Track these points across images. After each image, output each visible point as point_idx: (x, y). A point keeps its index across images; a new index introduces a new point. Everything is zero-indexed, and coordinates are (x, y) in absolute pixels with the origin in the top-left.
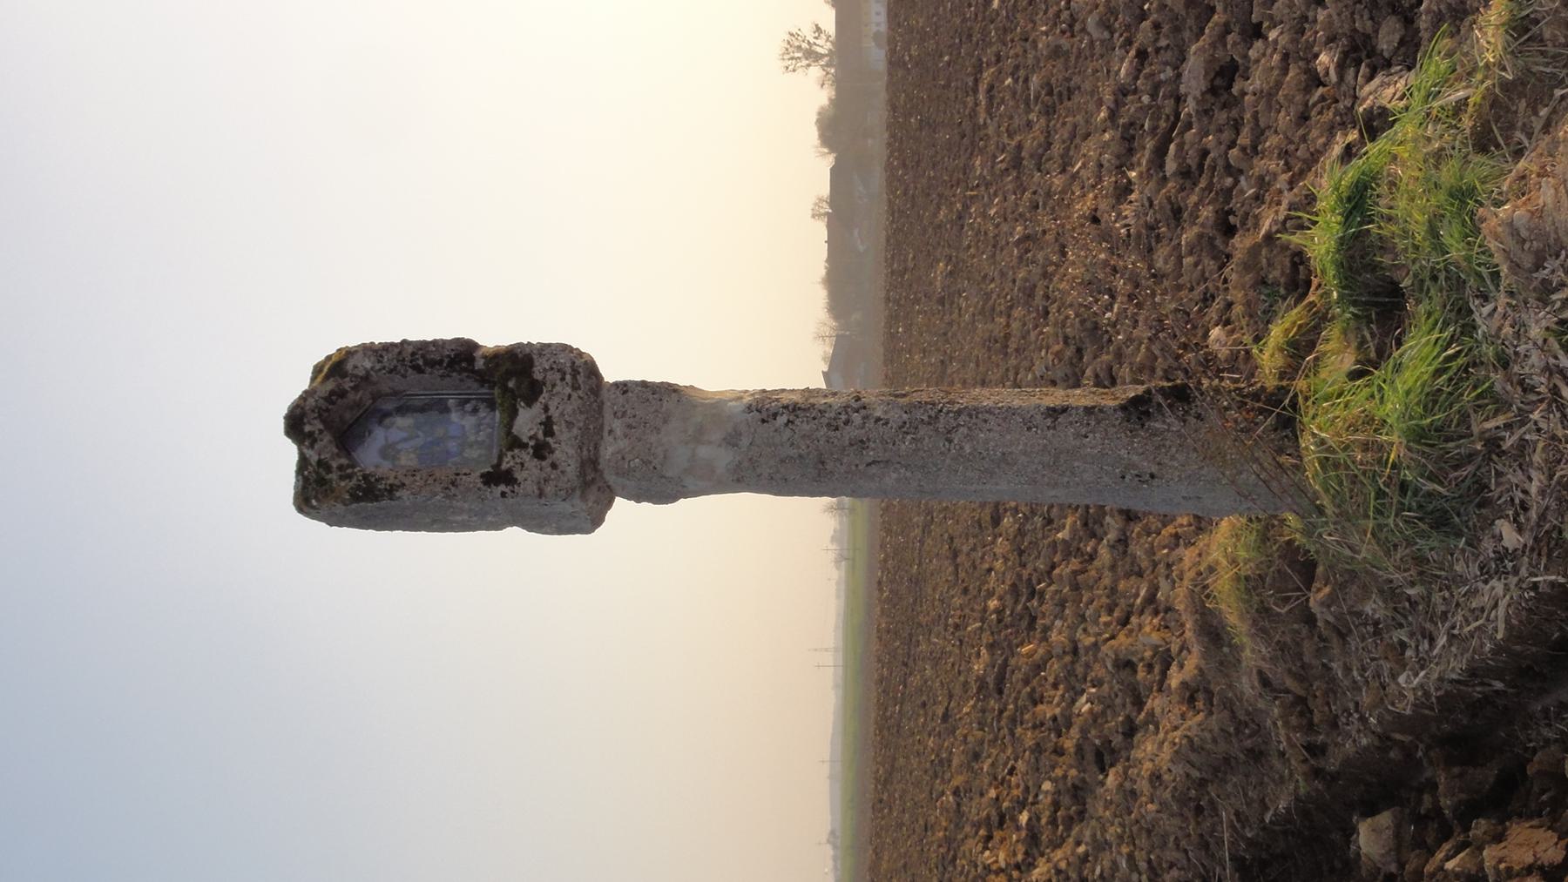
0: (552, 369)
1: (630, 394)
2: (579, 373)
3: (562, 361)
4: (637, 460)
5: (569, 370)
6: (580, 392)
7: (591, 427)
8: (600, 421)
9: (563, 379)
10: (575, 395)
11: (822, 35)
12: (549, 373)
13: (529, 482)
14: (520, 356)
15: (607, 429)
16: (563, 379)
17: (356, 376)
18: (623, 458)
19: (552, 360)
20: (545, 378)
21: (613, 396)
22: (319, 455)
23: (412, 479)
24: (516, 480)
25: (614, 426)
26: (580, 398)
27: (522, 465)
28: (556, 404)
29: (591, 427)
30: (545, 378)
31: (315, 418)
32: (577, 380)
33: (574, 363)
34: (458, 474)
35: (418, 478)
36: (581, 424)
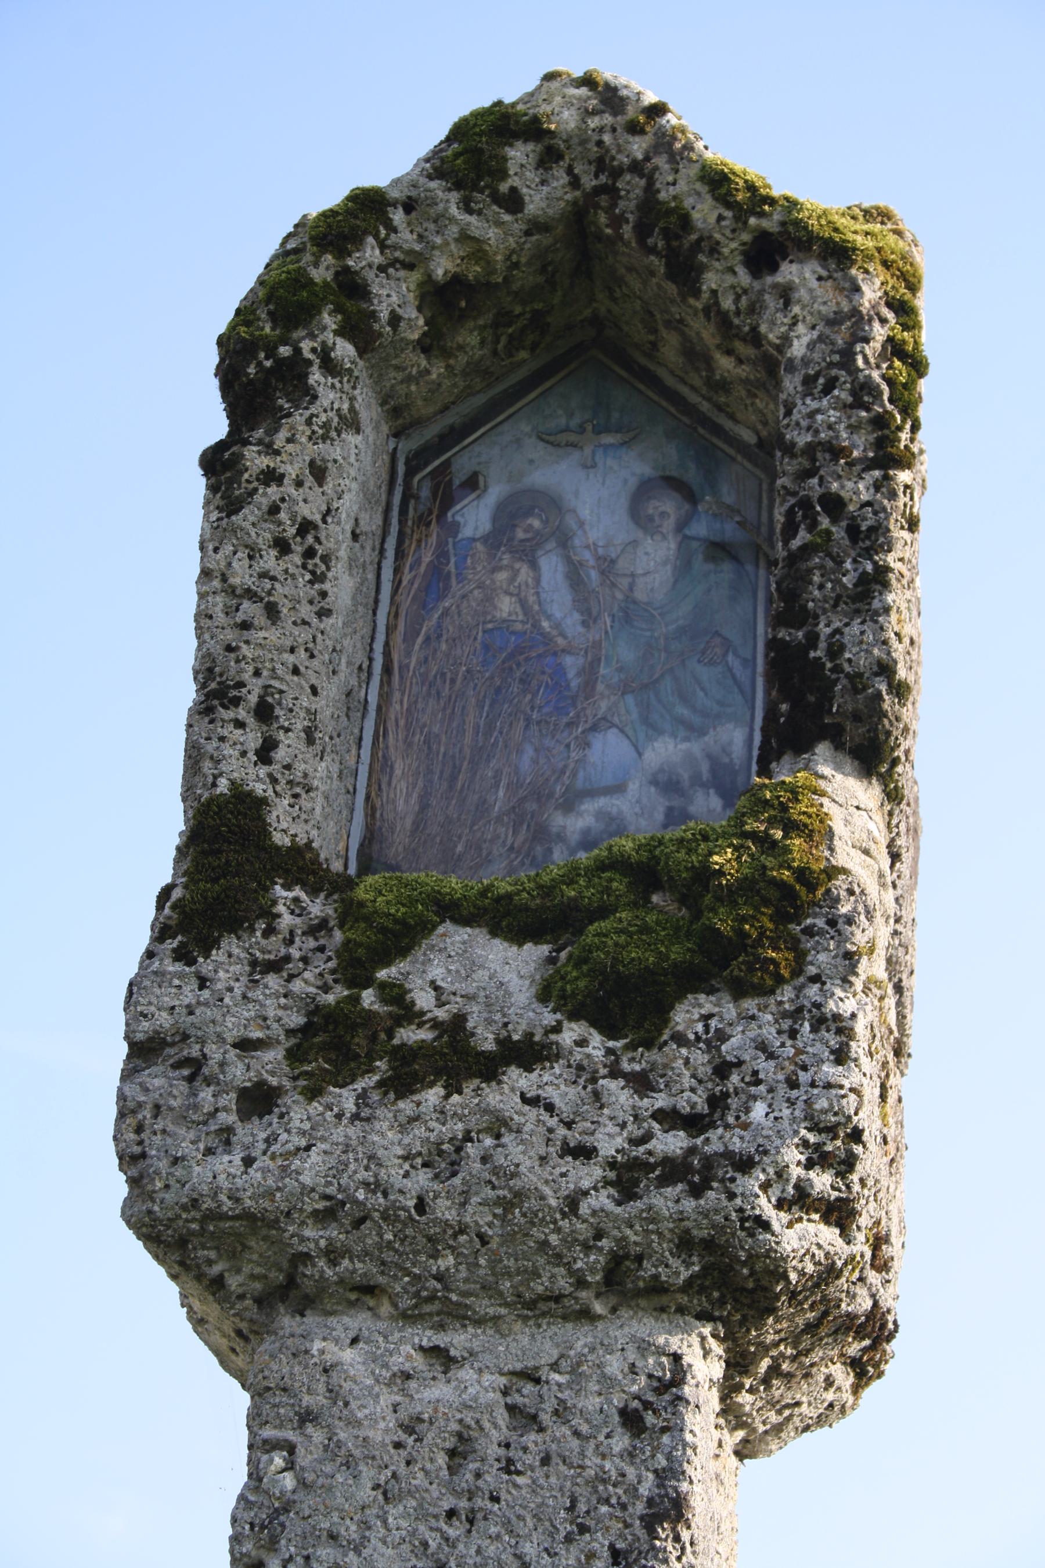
0: (722, 1069)
1: (621, 1442)
2: (696, 1191)
3: (759, 1110)
4: (288, 1481)
5: (715, 1141)
6: (603, 1200)
7: (447, 1261)
8: (485, 1306)
9: (669, 1118)
10: (588, 1175)
11: (220, 1105)
12: (700, 1057)
13: (189, 994)
14: (626, 880)
15: (457, 1340)
16: (669, 1118)
17: (755, 308)
18: (306, 1418)
19: (766, 1067)
20: (680, 1039)
21: (614, 1365)
22: (409, 206)
23: (263, 537)
24: (208, 946)
25: (467, 1374)
26: (572, 1203)
27: (274, 966)
28: (552, 1094)
29: (447, 1261)
30: (680, 1039)
31: (575, 183)
32: (665, 1181)
33: (745, 1165)
34: (264, 712)
35: (270, 561)
36: (444, 1210)
